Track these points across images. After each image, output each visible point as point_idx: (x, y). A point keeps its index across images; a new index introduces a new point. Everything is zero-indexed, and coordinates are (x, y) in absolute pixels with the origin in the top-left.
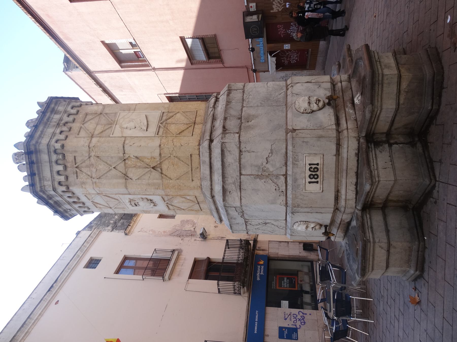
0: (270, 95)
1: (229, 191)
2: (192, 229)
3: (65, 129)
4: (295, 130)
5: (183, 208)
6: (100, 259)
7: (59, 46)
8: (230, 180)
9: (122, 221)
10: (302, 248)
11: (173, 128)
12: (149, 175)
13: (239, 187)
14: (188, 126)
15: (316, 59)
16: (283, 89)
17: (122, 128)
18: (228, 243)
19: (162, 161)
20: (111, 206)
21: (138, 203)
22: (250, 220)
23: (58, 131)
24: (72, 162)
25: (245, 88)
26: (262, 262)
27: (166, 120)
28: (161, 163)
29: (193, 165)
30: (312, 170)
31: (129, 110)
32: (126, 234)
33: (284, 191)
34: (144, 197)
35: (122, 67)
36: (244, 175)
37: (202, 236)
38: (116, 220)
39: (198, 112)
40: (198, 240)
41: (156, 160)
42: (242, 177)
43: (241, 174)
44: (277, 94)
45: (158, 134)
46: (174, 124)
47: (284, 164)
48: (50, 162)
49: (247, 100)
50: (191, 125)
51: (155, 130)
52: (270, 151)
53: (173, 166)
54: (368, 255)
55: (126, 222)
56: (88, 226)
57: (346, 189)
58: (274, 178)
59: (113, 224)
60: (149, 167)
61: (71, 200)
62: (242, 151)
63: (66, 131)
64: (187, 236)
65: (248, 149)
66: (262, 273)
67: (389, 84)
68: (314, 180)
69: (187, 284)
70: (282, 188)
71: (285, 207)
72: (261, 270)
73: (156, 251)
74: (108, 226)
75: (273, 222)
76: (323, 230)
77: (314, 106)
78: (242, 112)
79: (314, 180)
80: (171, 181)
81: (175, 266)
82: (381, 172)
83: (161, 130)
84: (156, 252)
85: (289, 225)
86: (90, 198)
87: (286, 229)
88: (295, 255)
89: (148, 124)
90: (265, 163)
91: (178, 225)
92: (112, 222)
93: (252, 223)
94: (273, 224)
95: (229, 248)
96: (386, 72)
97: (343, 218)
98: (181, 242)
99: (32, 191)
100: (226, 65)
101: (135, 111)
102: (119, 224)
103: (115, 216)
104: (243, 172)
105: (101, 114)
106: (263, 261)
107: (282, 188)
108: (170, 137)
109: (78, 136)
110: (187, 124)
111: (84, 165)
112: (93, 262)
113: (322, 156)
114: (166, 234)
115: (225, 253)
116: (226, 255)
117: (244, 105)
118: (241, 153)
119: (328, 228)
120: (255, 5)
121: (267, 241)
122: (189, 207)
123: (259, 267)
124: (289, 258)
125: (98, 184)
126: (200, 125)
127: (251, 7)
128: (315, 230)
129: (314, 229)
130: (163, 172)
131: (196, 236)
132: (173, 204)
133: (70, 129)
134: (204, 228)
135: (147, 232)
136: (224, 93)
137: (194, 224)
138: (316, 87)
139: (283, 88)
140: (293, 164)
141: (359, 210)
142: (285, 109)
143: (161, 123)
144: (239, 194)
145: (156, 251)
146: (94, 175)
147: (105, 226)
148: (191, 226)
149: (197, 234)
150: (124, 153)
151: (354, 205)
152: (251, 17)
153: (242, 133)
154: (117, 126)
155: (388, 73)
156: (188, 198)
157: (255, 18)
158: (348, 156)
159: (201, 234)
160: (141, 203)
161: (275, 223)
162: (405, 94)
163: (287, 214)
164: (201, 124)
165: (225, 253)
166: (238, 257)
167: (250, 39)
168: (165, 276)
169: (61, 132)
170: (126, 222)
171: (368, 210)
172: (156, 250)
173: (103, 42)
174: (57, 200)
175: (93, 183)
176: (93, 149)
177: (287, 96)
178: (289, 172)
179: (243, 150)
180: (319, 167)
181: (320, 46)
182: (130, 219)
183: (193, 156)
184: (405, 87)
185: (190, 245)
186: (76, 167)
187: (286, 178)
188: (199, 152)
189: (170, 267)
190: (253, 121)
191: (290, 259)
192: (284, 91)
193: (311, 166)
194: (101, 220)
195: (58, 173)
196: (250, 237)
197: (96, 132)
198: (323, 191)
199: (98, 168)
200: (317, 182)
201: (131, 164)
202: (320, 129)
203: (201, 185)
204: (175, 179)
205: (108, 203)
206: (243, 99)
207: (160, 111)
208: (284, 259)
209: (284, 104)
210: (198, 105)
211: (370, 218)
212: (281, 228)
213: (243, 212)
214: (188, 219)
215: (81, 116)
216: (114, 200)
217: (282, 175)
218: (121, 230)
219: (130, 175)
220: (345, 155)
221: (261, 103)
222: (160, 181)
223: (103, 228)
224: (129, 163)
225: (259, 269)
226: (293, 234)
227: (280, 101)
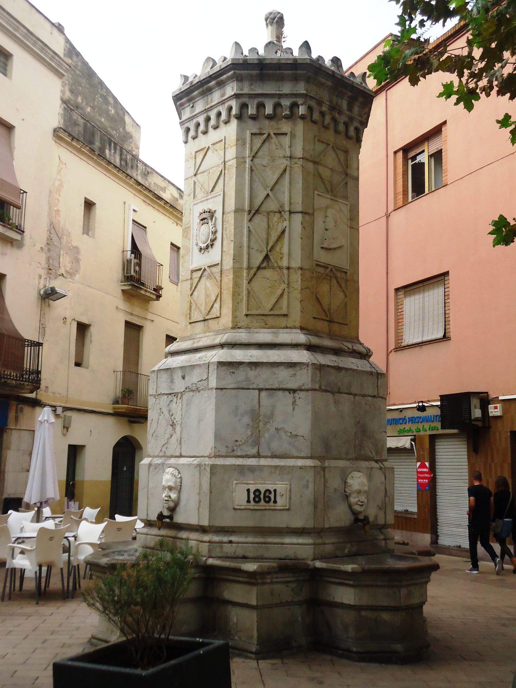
1: (235, 372)
3: (328, 119)
5: (195, 293)
6: (8, 73)
7: (440, 41)
8: (252, 373)
9: (81, 121)
11: (325, 288)
13: (240, 386)
14: (326, 310)
15: (398, 529)
16: (376, 455)
17: (327, 207)
18: (31, 346)
20: (198, 176)
21: (208, 223)
22: (179, 401)
24: (279, 129)
25: (381, 399)
27: (336, 278)
29: (271, 317)
30: (267, 494)
31: (351, 219)
33: (235, 453)
34: (219, 235)
35: (395, 153)
36: (259, 395)
37: (50, 292)
38: (82, 109)
39: (345, 326)
40: (39, 283)
41: (279, 261)
42: (257, 391)
43: (260, 390)
45: (317, 265)
46: (329, 290)
47: (274, 454)
48: (280, 96)
50: (328, 315)
51: (322, 261)
52: (294, 433)
55: (79, 131)
56: (72, 49)
61: (213, 114)
62: (295, 393)
63: (323, 121)
64: (48, 259)
65: (298, 402)
68: (252, 496)
71: (208, 454)
74: (71, 91)
76: (166, 513)
77: (355, 498)
83: (321, 270)
85: (173, 461)
86: (217, 146)
89: (330, 249)
91: (71, 240)
92: (80, 100)
93: (174, 404)
94: (171, 436)
96: (404, 591)
99: (235, 62)
100: (392, 356)
101: (349, 228)
102: (75, 116)
103: (91, 107)
104: (263, 394)
105: (347, 175)
109: (316, 140)
110: (329, 310)
113: (287, 507)
117: (357, 398)
120: (499, 415)
127: (496, 408)
128: (166, 501)
129: (166, 499)
131: (48, 279)
132: (203, 279)
133: (326, 128)
134: (65, 296)
136: (374, 368)
137: (71, 274)
140: (276, 467)
143: (331, 270)
144: (230, 387)
147: (71, 86)
148: (68, 269)
152: (478, 405)
154: (329, 202)
155: (401, 593)
156: (217, 306)
157: (477, 413)
158: (287, 544)
159: (53, 290)
160: (206, 229)
163: (195, 458)
167: (439, 403)
169: (323, 114)
170: (79, 131)
173: (445, 123)
174: (212, 93)
178: (263, 462)
179: (296, 395)
180: (272, 503)
181: (421, 535)
182: (84, 139)
183: (284, 319)
185: (30, 265)
186: (269, 135)
187: (254, 457)
188: (290, 328)
193: (273, 493)
195: (261, 106)
197: (321, 169)
198: (234, 509)
199: (267, 169)
200: (248, 501)
201: (274, 222)
202: (324, 505)
203: (239, 328)
205: (205, 174)
207: (348, 268)
212: (164, 449)
213: (198, 390)
214: (81, 262)
216: (212, 185)
217: (258, 450)
218: (65, 120)
219: (258, 219)
220: (287, 540)
226: (151, 468)
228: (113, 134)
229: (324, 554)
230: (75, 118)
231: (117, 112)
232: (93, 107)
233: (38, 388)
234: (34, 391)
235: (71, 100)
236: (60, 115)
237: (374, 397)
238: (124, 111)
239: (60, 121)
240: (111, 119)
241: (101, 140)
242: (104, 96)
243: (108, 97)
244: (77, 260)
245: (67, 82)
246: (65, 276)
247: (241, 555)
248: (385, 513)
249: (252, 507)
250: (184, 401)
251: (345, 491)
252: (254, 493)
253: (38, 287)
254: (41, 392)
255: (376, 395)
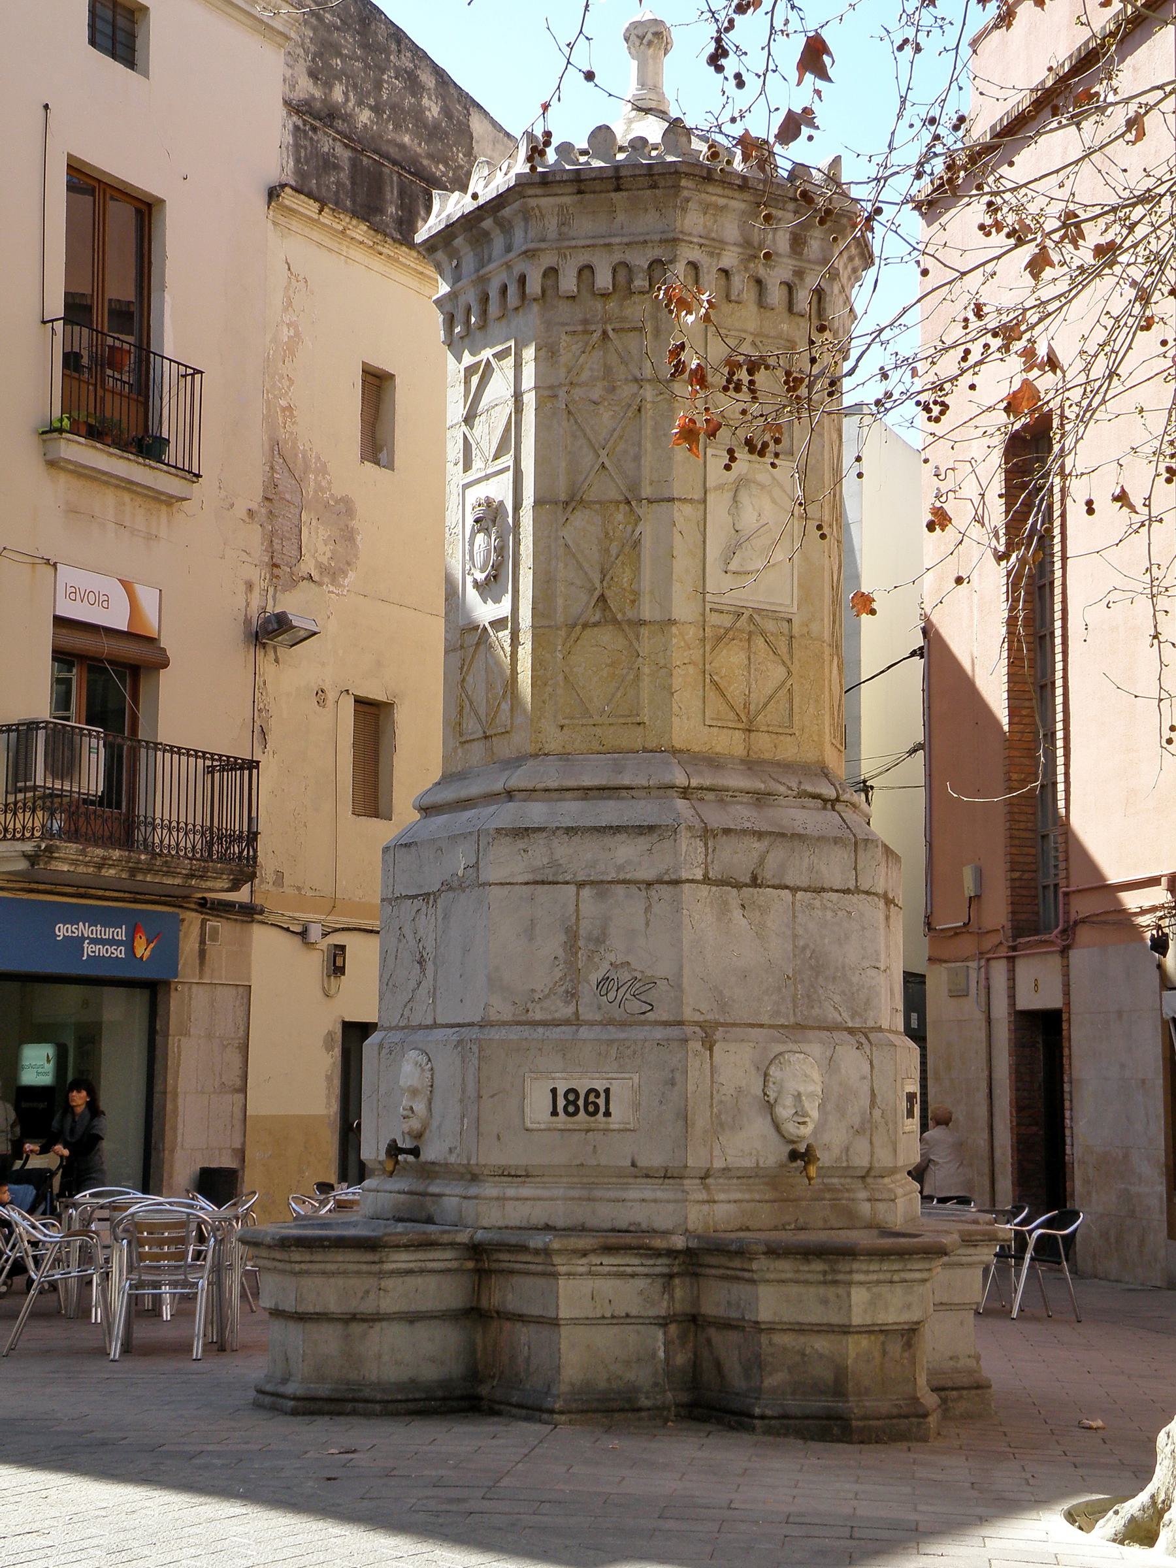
0: (834, 978)
2: (308, 566)
4: (711, 1050)
5: (470, 679)
8: (563, 849)
9: (343, 154)
10: (214, 1165)
11: (731, 659)
12: (578, 582)
13: (539, 878)
16: (852, 1017)
19: (626, 627)
22: (431, 911)
23: (729, 259)
26: (142, 949)
27: (763, 633)
28: (615, 622)
30: (592, 1098)
32: (273, 194)
36: (578, 894)
38: (348, 118)
42: (572, 889)
43: (581, 885)
44: (837, 998)
46: (746, 662)
49: (817, 903)
53: (607, 665)
54: (340, 1259)
55: (338, 183)
57: (534, 1199)
58: (568, 985)
59: (324, 101)
60: (605, 583)
64: (270, 538)
65: (656, 909)
66: (89, 949)
67: (825, 1302)
68: (561, 1102)
69: (30, 560)
70: (537, 1010)
72: (103, 942)
73: (193, 375)
74: (313, 74)
75: (427, 984)
78: (774, 887)
79: (561, 1102)
80: (560, 656)
81: (117, 486)
82: (588, 1285)
84: (185, 376)
87: (403, 1028)
88: (180, 1126)
90: (612, 957)
91: (330, 483)
92: (338, 94)
95: (211, 770)
97: (445, 1199)
98: (240, 511)
99: (524, 180)
102: (326, 143)
103: (371, 108)
104: (586, 892)
106: (147, 953)
107: (537, 1010)
108: (701, 651)
111: (613, 359)
112: (121, 22)
114: (280, 420)
115: (189, 755)
116: (184, 758)
118: (643, 886)
119: (411, 1158)
121: (249, 979)
122: (471, 703)
123: (121, 934)
124: (165, 1093)
125: (549, 405)
126: (742, 747)
130: (588, 631)
134: (315, 633)
135: (285, 310)
137: (333, 572)
138: (856, 1121)
139: (857, 1019)
141: (472, 1238)
142: (782, 1021)
144: (521, 879)
145: (193, 375)
146: (577, 393)
147: (313, 60)
148: (324, 560)
149: (284, 591)
150: (650, 501)
151: (485, 1223)
153: (704, 890)
158: (632, 1201)
161: (423, 991)
162: (797, 1348)
164: (745, 753)
165: (189, 755)
166: (174, 824)
168: (69, 440)
170: (338, 183)
171: (470, 1265)
172: (198, 377)
175: (551, 387)
176: (666, 396)
177: (827, 1029)
178: (584, 1032)
179: (653, 893)
182: (354, 202)
184: (817, 1346)
185: (223, 557)
187: (567, 1022)
188: (651, 751)
189: (114, 460)
190: (744, 922)
191: (157, 1096)
192: (848, 1020)
193: (603, 1095)
194: (345, 26)
195: (587, 270)
196: (269, 887)
199: (602, 409)
200: (555, 1113)
204: (567, 670)
206: (823, 890)
208: (158, 1066)
209: (799, 1019)
210: (816, 739)
211: (449, 1270)
213: (462, 888)
215: (785, 327)
218: (297, 161)
221: (804, 948)
222: (560, 618)
223: (302, 45)
224: (620, 517)
225: (108, 933)
226: (384, 1052)
227: (813, 1007)
228: (439, 174)
229: (711, 1223)
230: (326, 149)
231: (447, 112)
232: (377, 109)
233: (252, 877)
234: (246, 882)
235: (313, 98)
236: (284, 149)
237: (847, 891)
238: (470, 104)
239: (285, 164)
240: (433, 133)
241: (402, 199)
242: (406, 72)
243: (419, 72)
244: (348, 536)
245: (300, 51)
246: (316, 578)
247: (541, 1223)
248: (871, 1143)
249: (560, 1126)
250: (439, 911)
251: (765, 1094)
252: (566, 1095)
253: (246, 615)
254: (264, 887)
255: (852, 888)
